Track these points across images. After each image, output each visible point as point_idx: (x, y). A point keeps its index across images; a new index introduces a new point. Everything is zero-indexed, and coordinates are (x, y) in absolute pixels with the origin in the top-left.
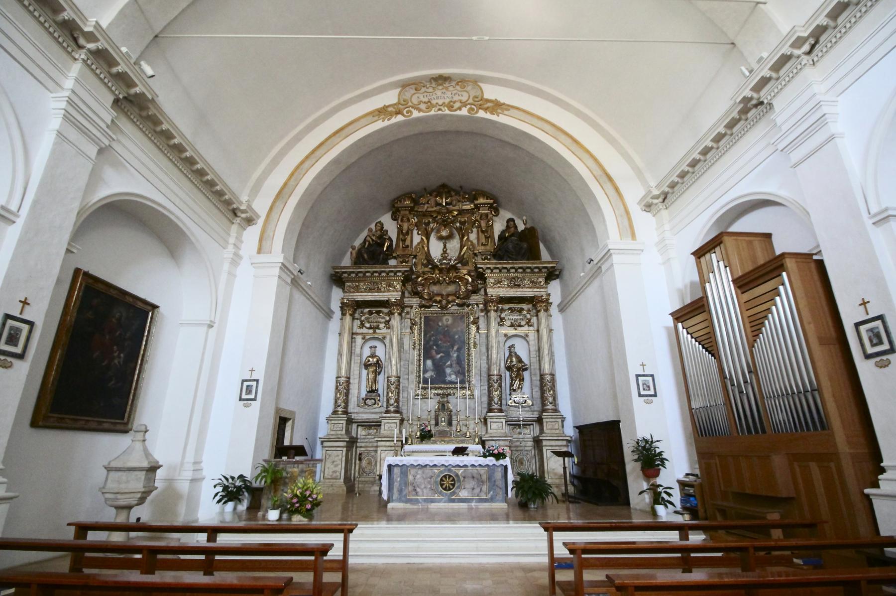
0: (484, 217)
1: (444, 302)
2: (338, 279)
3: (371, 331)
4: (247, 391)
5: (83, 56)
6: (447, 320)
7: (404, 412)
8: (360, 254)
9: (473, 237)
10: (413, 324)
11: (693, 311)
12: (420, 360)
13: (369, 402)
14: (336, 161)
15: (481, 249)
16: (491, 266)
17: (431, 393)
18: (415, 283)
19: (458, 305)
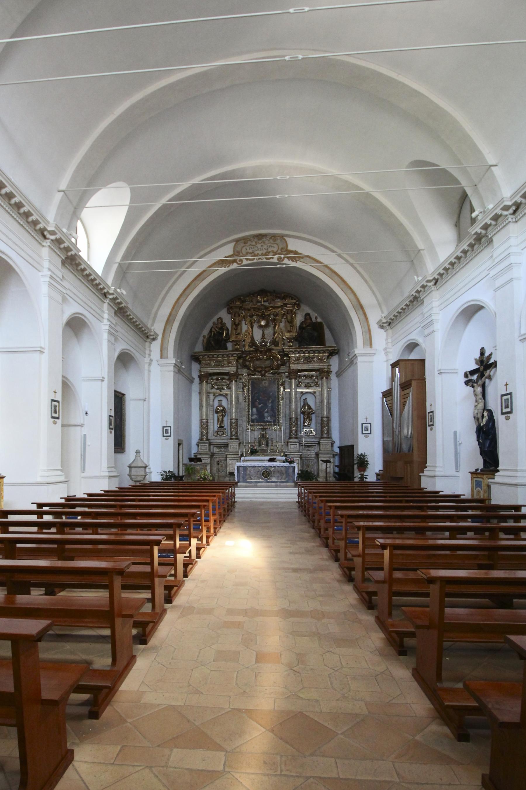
0: (289, 312)
1: (263, 372)
2: (195, 358)
3: (218, 391)
4: (166, 432)
6: (265, 383)
7: (241, 438)
9: (282, 325)
10: (244, 386)
11: (387, 394)
12: (249, 408)
13: (220, 433)
15: (287, 335)
16: (293, 350)
17: (256, 427)
18: (245, 360)
19: (272, 373)
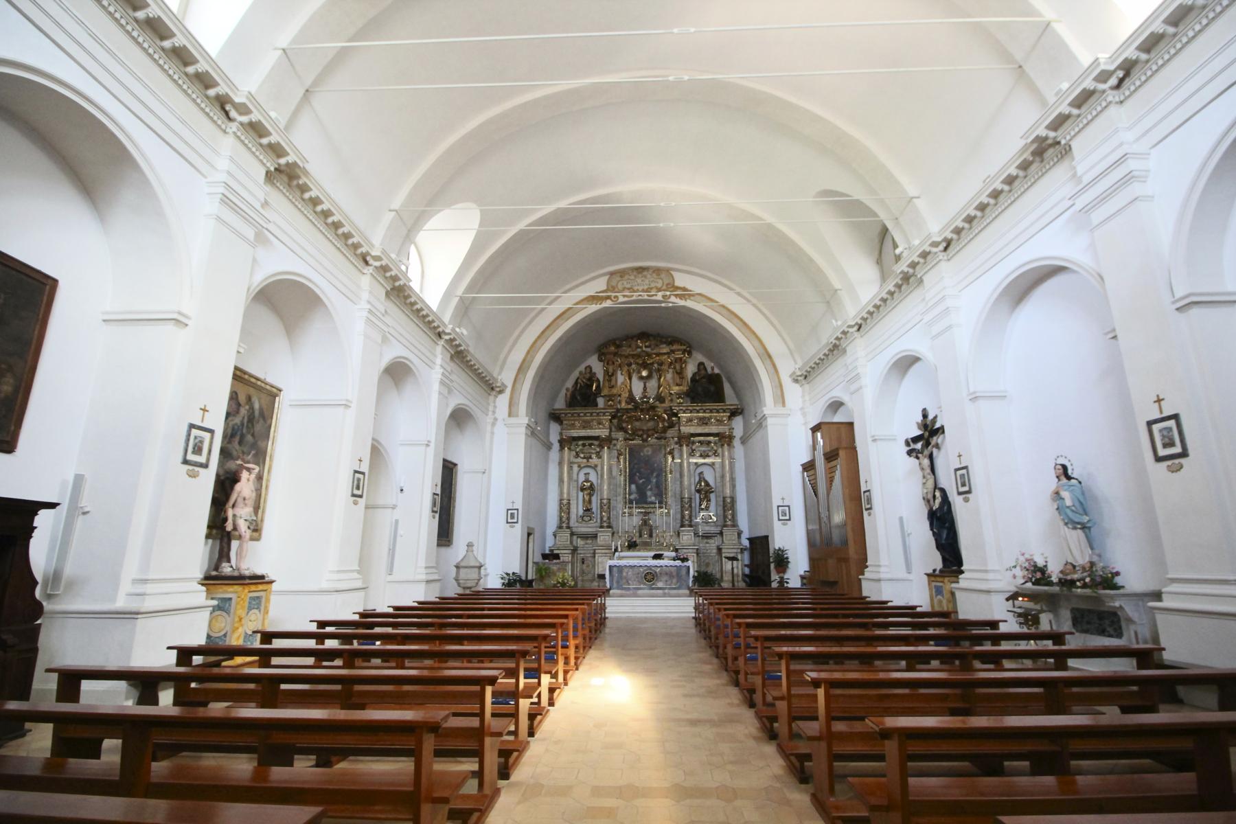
2: (555, 417)
5: (234, 129)
8: (573, 396)
10: (620, 454)
11: (809, 467)
14: (560, 339)
15: (675, 389)
17: (636, 511)
18: (620, 420)
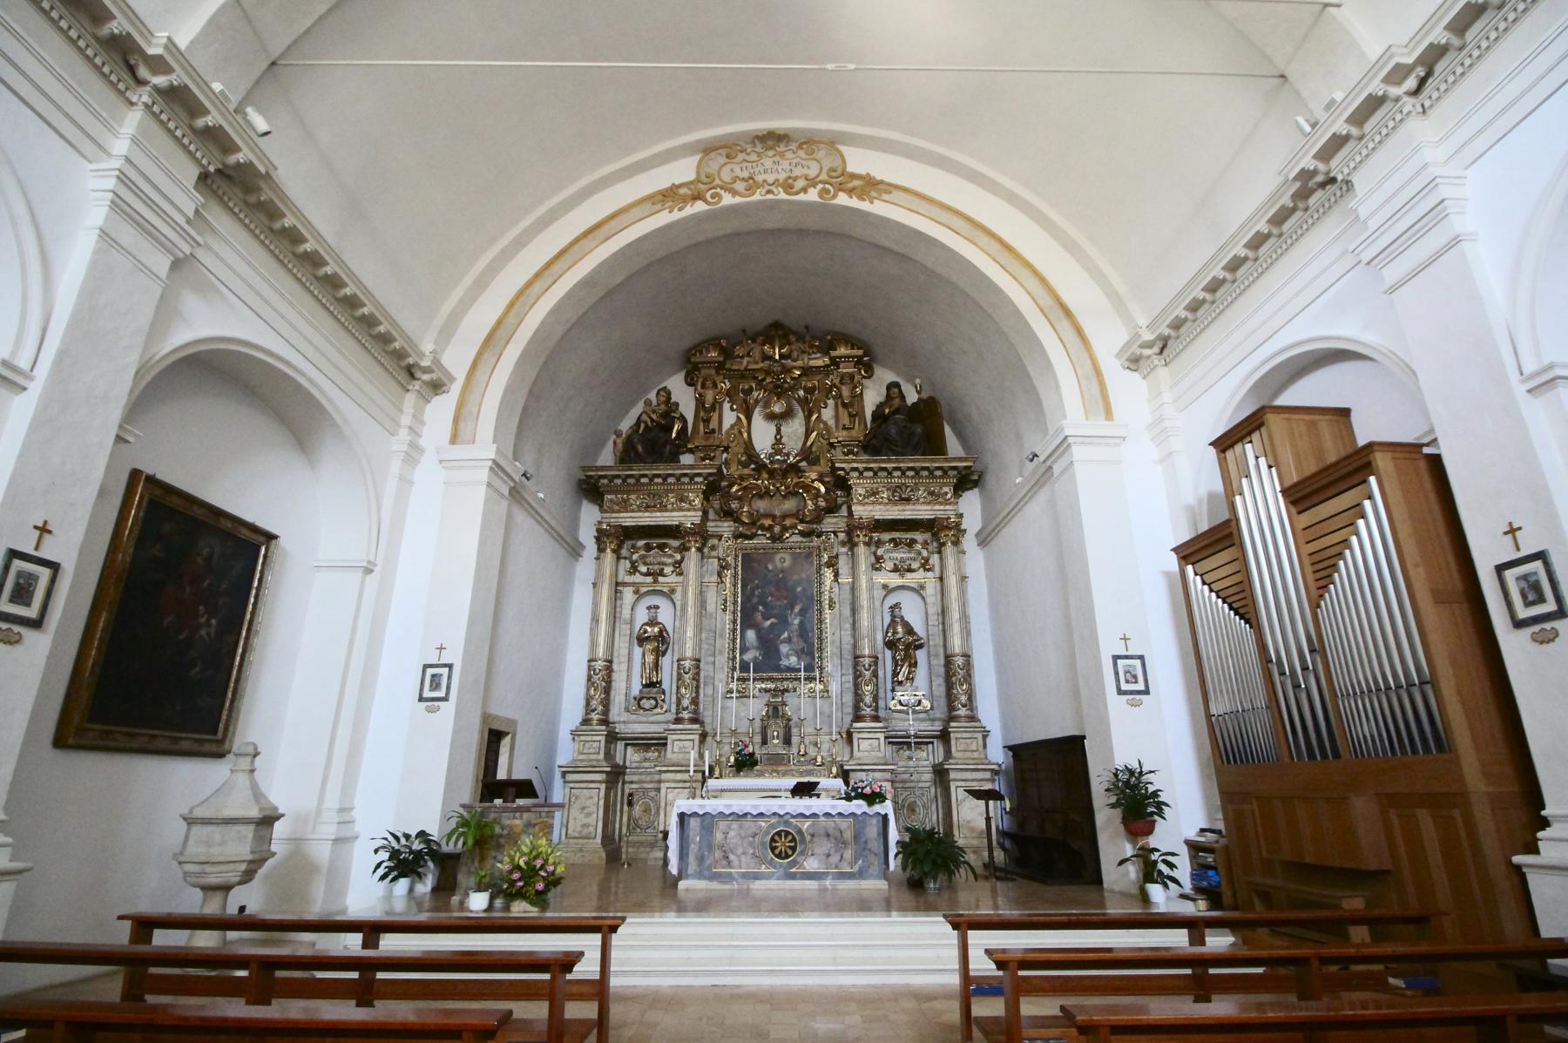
0: (847, 379)
1: (777, 529)
2: (591, 488)
3: (649, 579)
4: (433, 684)
5: (145, 98)
6: (783, 560)
7: (707, 720)
8: (629, 444)
9: (828, 414)
10: (723, 567)
11: (1213, 545)
12: (734, 630)
13: (646, 704)
14: (588, 282)
15: (842, 435)
16: (860, 466)
17: (754, 687)
18: (727, 496)
19: (802, 534)
